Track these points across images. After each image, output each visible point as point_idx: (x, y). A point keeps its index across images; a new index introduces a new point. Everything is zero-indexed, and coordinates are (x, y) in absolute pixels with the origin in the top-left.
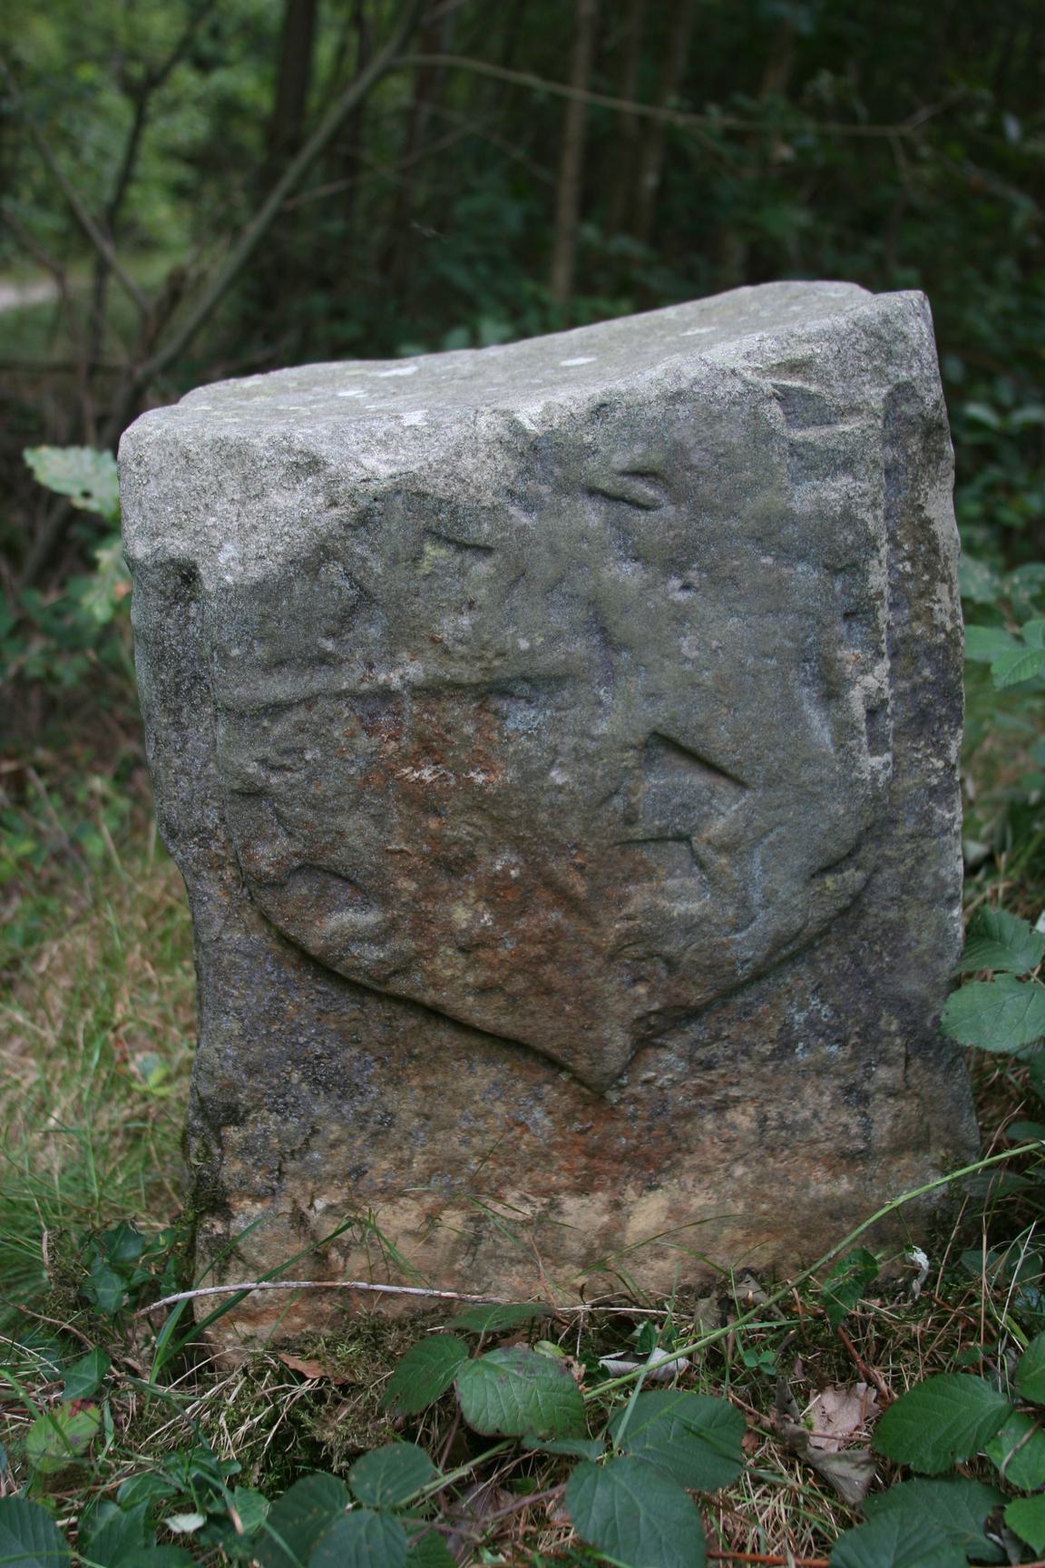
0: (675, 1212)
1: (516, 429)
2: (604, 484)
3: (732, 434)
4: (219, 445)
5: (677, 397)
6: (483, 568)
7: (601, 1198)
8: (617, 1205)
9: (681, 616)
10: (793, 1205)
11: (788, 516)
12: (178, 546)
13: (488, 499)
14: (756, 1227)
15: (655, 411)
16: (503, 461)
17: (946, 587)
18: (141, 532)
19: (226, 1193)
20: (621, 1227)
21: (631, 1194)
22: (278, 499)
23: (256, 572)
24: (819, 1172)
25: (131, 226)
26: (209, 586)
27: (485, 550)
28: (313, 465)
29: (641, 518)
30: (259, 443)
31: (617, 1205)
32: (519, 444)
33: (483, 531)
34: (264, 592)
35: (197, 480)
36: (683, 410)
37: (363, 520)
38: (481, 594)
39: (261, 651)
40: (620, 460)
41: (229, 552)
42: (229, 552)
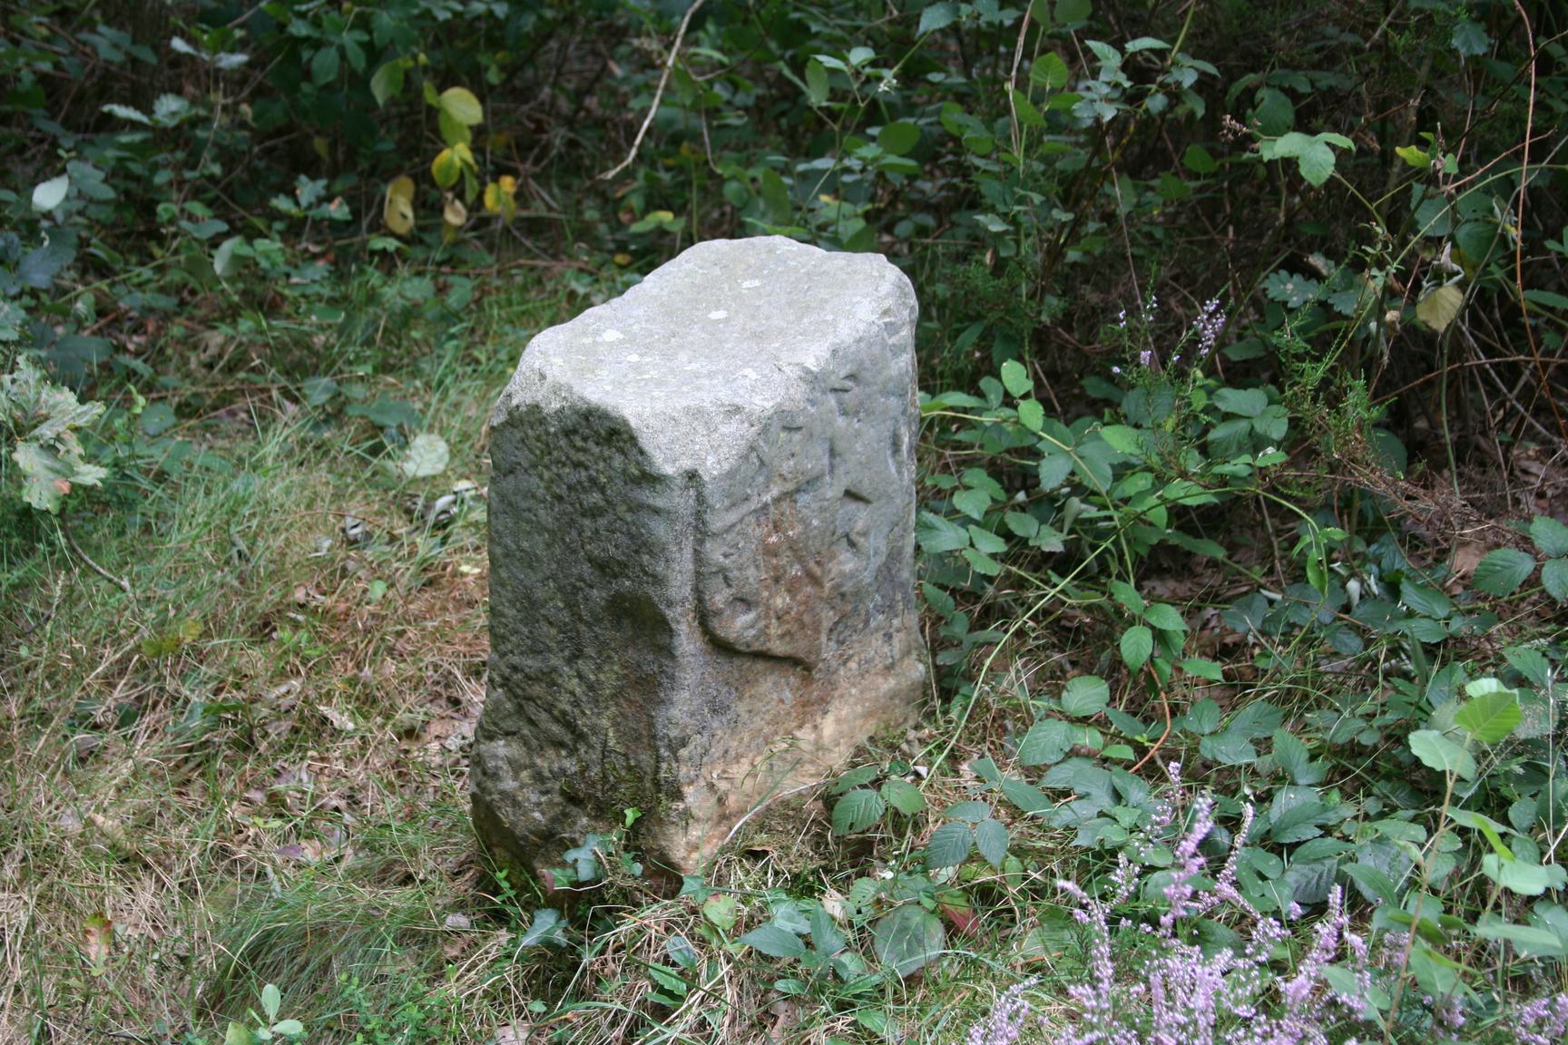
0: (838, 721)
1: (808, 372)
2: (837, 386)
3: (876, 350)
4: (687, 410)
5: (860, 340)
6: (797, 437)
7: (808, 726)
8: (815, 727)
9: (858, 434)
10: (877, 699)
11: (891, 379)
12: (687, 463)
13: (802, 405)
14: (868, 715)
15: (853, 349)
16: (804, 387)
17: (66, 52)
18: (666, 461)
19: (1224, 687)
20: (821, 737)
21: (819, 720)
22: (724, 429)
23: (726, 466)
24: (880, 680)
25: (385, 226)
26: (706, 478)
27: (799, 429)
28: (737, 409)
29: (846, 396)
30: (707, 404)
31: (815, 727)
32: (810, 377)
33: (800, 421)
34: (731, 474)
35: (683, 429)
36: (862, 345)
37: (765, 430)
38: (797, 449)
39: (727, 503)
40: (843, 373)
41: (711, 460)
42: (711, 460)
